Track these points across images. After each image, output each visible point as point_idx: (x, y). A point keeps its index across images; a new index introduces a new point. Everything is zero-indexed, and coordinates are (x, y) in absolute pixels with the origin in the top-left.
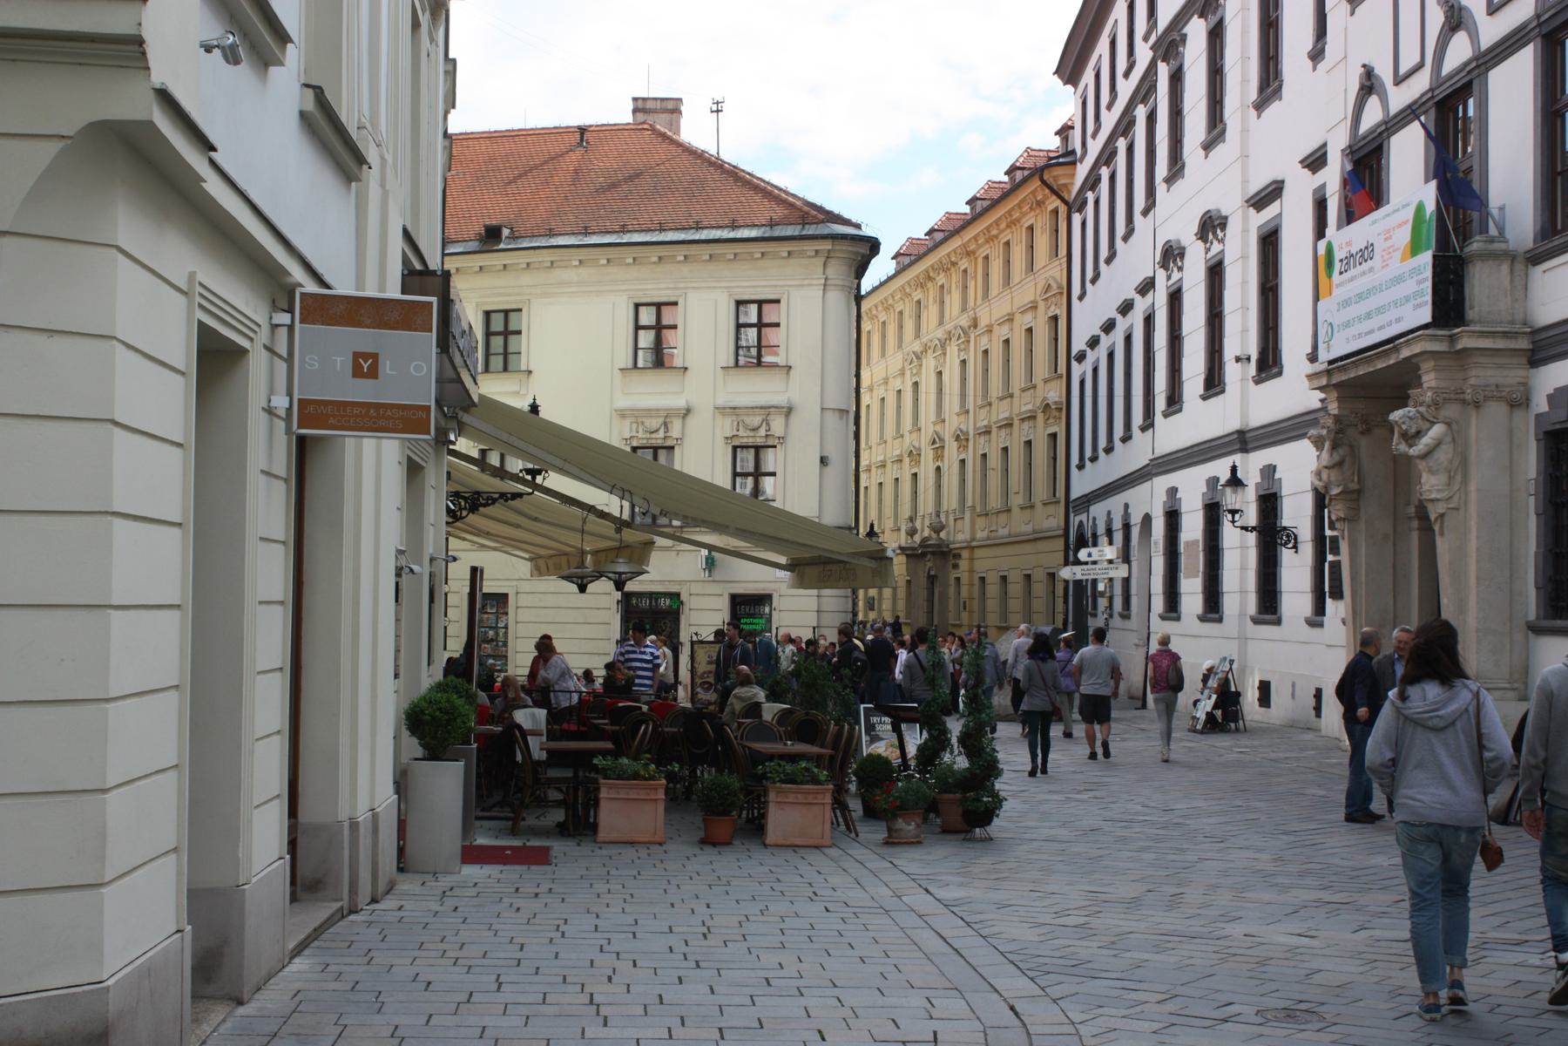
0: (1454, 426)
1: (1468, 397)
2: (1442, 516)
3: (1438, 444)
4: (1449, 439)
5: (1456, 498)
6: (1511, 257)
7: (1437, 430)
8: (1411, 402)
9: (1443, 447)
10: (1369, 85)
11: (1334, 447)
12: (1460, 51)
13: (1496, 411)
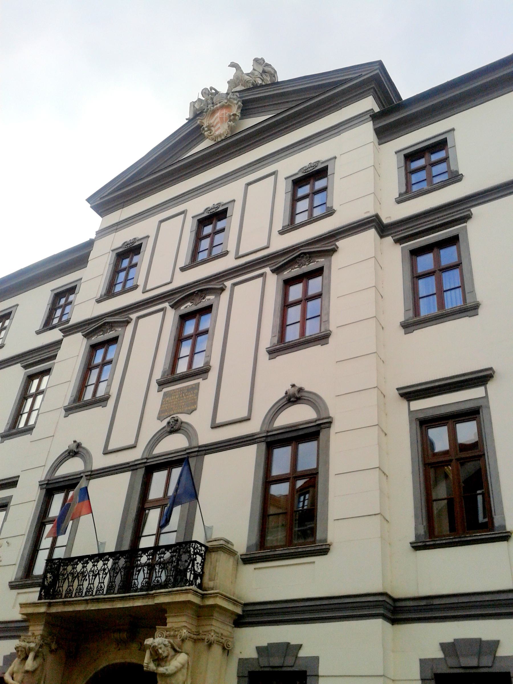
7: (182, 658)
10: (75, 451)
11: (35, 657)
13: (217, 650)
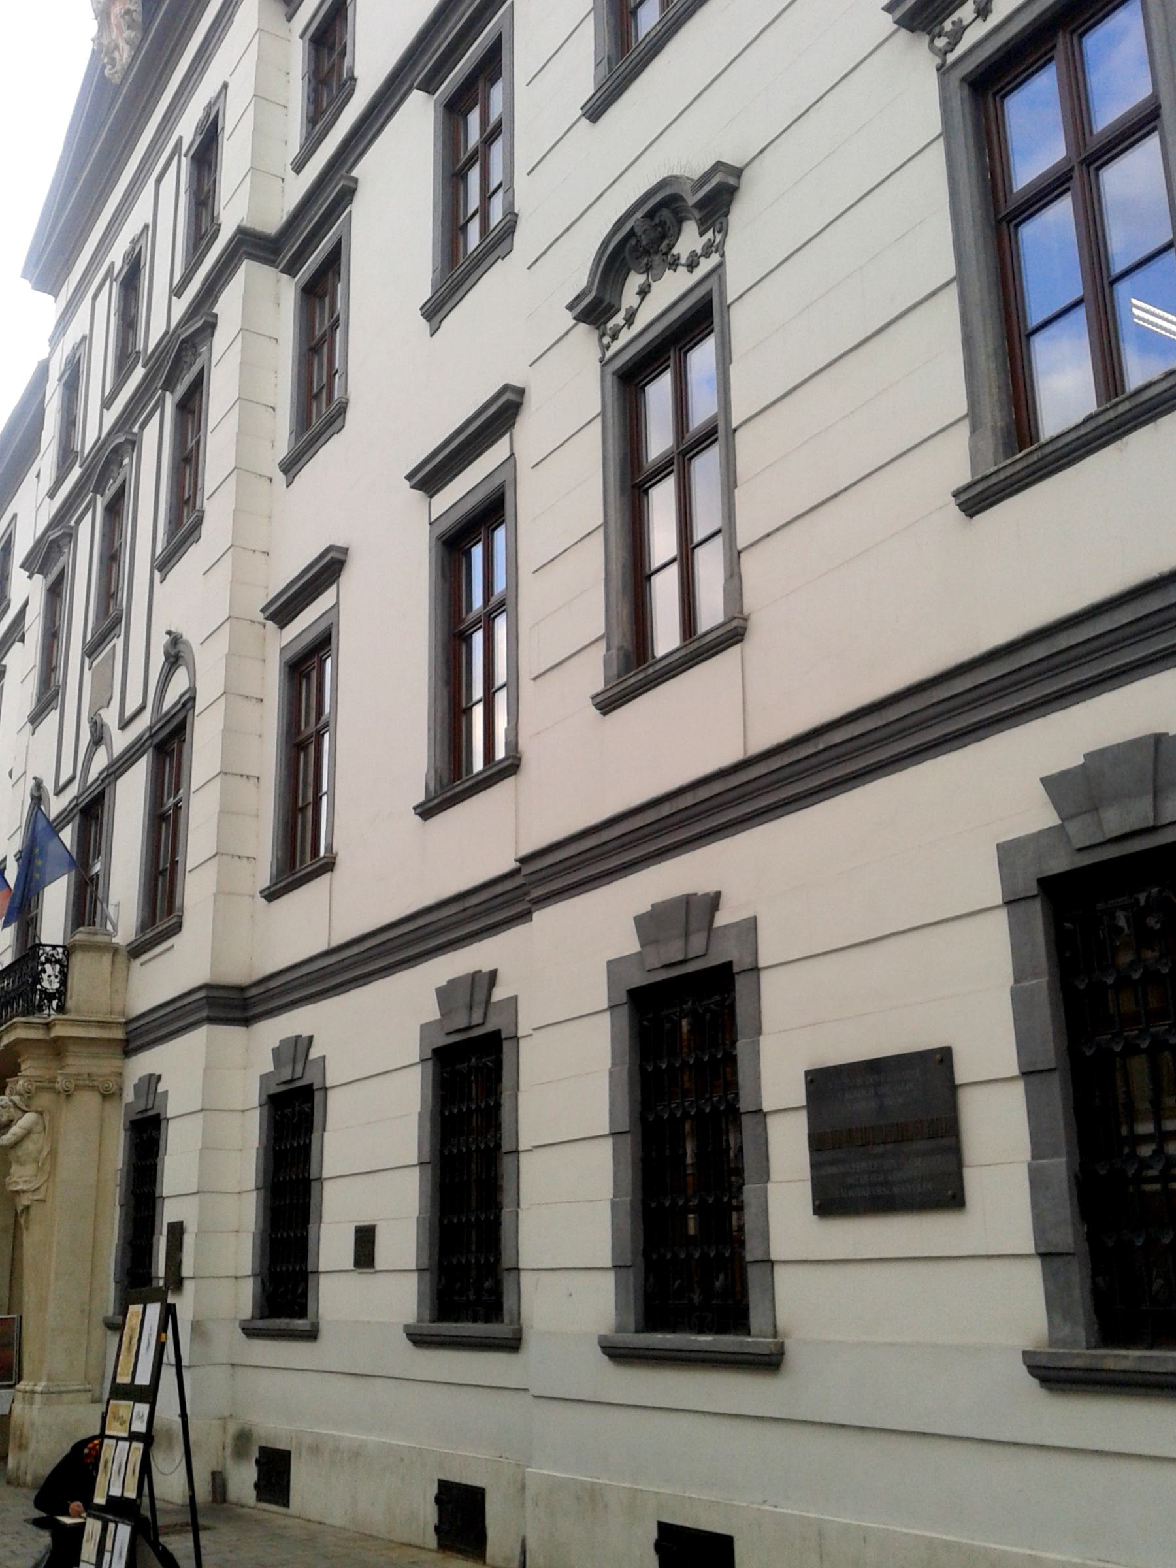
0: (47, 1117)
1: (57, 1086)
2: (28, 1208)
3: (28, 1133)
4: (39, 1128)
5: (43, 1189)
6: (115, 950)
7: (28, 1119)
8: (8, 1091)
9: (34, 1137)
12: (101, 760)
13: (88, 1101)
